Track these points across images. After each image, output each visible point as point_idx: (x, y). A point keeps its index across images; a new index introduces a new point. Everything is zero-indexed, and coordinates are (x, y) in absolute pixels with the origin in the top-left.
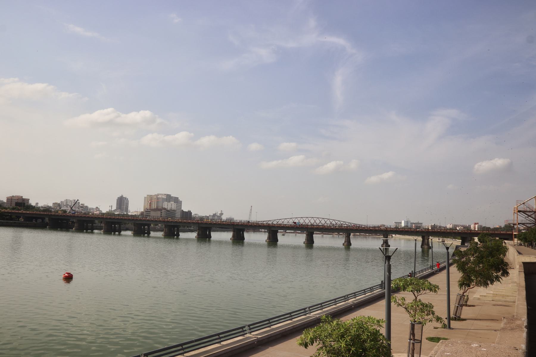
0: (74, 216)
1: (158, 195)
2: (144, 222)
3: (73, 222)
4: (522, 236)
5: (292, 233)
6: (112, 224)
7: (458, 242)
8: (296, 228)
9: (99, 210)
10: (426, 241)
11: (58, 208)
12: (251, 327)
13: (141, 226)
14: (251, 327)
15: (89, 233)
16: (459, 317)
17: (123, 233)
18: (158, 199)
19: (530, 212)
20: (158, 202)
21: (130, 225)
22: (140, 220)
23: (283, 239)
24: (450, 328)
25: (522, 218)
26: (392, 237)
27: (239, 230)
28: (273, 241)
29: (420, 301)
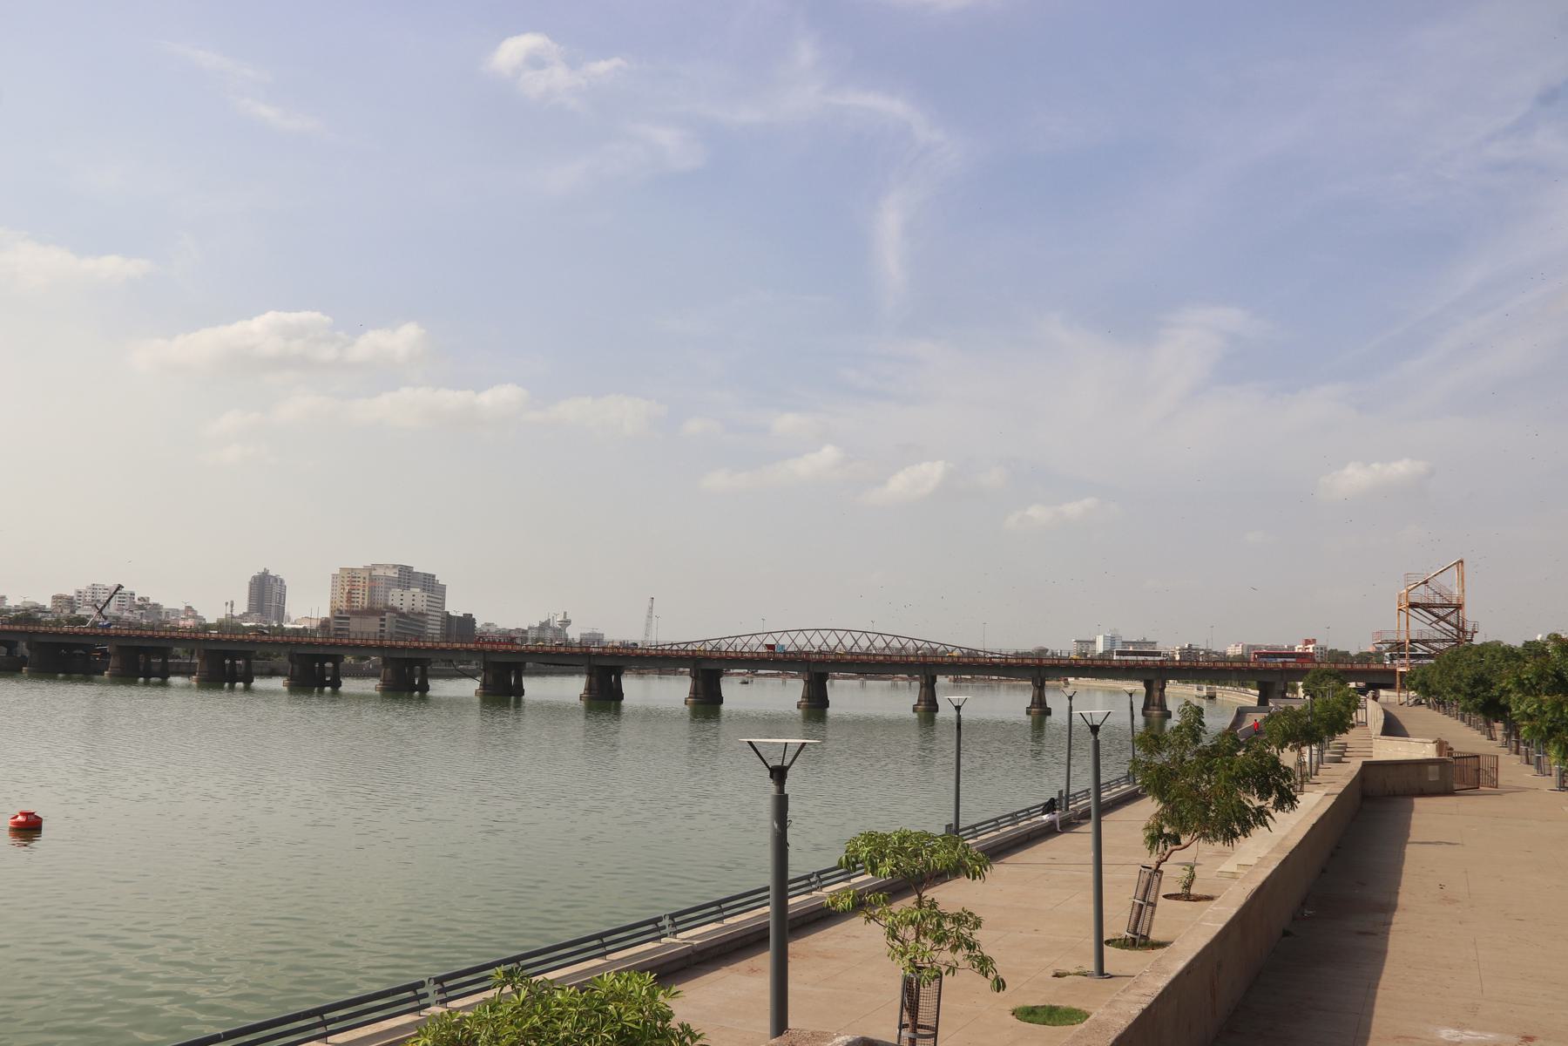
0: (108, 636)
1: (374, 567)
2: (321, 651)
3: (104, 654)
4: (1418, 678)
5: (772, 675)
6: (225, 658)
7: (1250, 697)
8: (774, 661)
9: (195, 617)
10: (1157, 694)
11: (67, 611)
12: (447, 984)
13: (313, 664)
14: (447, 984)
15: (157, 685)
16: (1146, 937)
17: (258, 683)
18: (373, 579)
19: (1442, 606)
20: (372, 590)
21: (283, 661)
22: (322, 645)
23: (735, 693)
24: (1101, 972)
25: (1420, 626)
26: (1067, 684)
27: (605, 671)
28: (707, 701)
29: (933, 904)
